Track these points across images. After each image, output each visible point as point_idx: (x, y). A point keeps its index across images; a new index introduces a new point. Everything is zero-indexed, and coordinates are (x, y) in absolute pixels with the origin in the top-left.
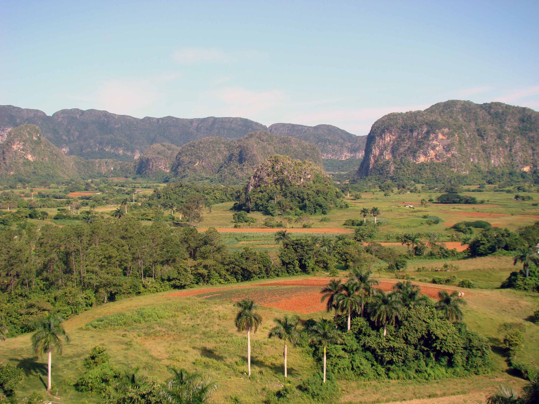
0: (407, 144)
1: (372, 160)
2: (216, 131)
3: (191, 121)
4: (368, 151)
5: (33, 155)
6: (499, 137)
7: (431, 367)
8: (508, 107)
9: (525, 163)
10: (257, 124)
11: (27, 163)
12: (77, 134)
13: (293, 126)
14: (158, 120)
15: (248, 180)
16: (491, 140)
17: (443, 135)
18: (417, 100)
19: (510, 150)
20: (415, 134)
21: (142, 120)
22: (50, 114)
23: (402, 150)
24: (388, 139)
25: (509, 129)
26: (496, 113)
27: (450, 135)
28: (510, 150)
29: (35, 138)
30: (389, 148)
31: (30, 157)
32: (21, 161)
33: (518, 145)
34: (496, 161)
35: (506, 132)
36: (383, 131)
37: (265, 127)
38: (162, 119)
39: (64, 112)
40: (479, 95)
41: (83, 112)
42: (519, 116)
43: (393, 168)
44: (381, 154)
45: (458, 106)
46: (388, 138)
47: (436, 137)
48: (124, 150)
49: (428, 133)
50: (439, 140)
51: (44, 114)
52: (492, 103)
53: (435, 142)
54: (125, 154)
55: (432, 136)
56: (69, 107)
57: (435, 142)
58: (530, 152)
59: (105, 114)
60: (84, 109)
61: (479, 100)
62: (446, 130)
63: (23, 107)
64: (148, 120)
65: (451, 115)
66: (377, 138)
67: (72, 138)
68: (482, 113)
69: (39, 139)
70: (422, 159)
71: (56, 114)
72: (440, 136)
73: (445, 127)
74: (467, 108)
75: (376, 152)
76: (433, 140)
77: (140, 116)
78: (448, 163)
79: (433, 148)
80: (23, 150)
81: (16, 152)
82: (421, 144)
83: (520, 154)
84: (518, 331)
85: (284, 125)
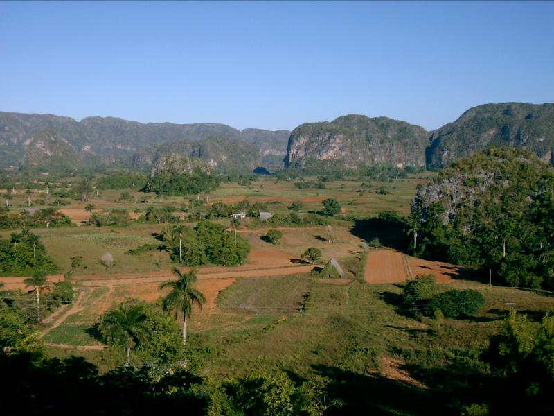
0: (315, 145)
1: (291, 157)
2: (202, 133)
3: (183, 126)
4: (288, 150)
5: (51, 151)
6: (382, 142)
7: (319, 337)
8: (391, 120)
9: (400, 161)
10: (232, 129)
11: (46, 157)
12: (98, 135)
13: (260, 130)
14: (159, 125)
15: (501, 155)
16: (375, 143)
17: (340, 139)
18: (326, 114)
19: (390, 152)
20: (321, 139)
21: (147, 125)
22: (78, 120)
23: (311, 150)
24: (301, 142)
25: (390, 137)
26: (383, 124)
27: (345, 140)
28: (390, 152)
29: (52, 139)
30: (303, 148)
31: (48, 152)
32: (42, 155)
33: (395, 148)
34: (380, 159)
35: (387, 138)
36: (298, 136)
37: (238, 131)
38: (162, 124)
39: (89, 119)
40: (372, 111)
41: (103, 119)
42: (397, 127)
43: (304, 163)
44: (297, 152)
45: (356, 119)
46: (303, 141)
47: (335, 141)
48: (131, 147)
49: (329, 137)
50: (337, 142)
51: (74, 120)
52: (381, 118)
53: (334, 145)
54: (131, 150)
55: (332, 140)
56: (93, 115)
57: (334, 145)
58: (403, 153)
59: (120, 121)
60: (104, 117)
61: (371, 115)
62: (342, 136)
63: (59, 115)
64: (151, 125)
65: (349, 125)
66: (295, 141)
67: (93, 138)
68: (372, 125)
69: (56, 139)
70: (325, 157)
71: (83, 120)
72: (338, 140)
73: (341, 133)
74: (362, 120)
75: (293, 151)
76: (332, 143)
77: (146, 122)
78: (342, 161)
79: (333, 149)
80: (43, 147)
81: (39, 149)
82: (324, 146)
83: (396, 155)
84: (523, 160)
85: (253, 129)
